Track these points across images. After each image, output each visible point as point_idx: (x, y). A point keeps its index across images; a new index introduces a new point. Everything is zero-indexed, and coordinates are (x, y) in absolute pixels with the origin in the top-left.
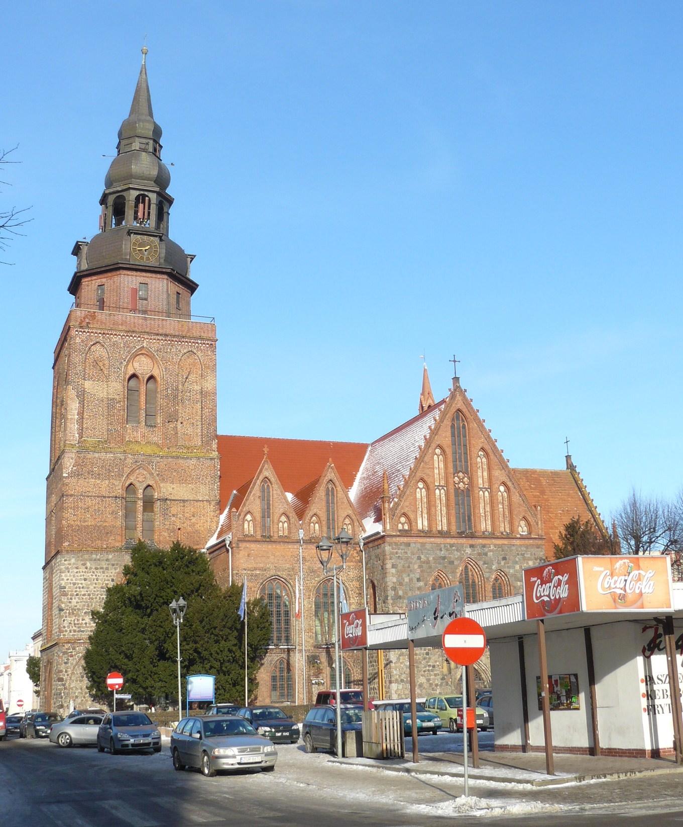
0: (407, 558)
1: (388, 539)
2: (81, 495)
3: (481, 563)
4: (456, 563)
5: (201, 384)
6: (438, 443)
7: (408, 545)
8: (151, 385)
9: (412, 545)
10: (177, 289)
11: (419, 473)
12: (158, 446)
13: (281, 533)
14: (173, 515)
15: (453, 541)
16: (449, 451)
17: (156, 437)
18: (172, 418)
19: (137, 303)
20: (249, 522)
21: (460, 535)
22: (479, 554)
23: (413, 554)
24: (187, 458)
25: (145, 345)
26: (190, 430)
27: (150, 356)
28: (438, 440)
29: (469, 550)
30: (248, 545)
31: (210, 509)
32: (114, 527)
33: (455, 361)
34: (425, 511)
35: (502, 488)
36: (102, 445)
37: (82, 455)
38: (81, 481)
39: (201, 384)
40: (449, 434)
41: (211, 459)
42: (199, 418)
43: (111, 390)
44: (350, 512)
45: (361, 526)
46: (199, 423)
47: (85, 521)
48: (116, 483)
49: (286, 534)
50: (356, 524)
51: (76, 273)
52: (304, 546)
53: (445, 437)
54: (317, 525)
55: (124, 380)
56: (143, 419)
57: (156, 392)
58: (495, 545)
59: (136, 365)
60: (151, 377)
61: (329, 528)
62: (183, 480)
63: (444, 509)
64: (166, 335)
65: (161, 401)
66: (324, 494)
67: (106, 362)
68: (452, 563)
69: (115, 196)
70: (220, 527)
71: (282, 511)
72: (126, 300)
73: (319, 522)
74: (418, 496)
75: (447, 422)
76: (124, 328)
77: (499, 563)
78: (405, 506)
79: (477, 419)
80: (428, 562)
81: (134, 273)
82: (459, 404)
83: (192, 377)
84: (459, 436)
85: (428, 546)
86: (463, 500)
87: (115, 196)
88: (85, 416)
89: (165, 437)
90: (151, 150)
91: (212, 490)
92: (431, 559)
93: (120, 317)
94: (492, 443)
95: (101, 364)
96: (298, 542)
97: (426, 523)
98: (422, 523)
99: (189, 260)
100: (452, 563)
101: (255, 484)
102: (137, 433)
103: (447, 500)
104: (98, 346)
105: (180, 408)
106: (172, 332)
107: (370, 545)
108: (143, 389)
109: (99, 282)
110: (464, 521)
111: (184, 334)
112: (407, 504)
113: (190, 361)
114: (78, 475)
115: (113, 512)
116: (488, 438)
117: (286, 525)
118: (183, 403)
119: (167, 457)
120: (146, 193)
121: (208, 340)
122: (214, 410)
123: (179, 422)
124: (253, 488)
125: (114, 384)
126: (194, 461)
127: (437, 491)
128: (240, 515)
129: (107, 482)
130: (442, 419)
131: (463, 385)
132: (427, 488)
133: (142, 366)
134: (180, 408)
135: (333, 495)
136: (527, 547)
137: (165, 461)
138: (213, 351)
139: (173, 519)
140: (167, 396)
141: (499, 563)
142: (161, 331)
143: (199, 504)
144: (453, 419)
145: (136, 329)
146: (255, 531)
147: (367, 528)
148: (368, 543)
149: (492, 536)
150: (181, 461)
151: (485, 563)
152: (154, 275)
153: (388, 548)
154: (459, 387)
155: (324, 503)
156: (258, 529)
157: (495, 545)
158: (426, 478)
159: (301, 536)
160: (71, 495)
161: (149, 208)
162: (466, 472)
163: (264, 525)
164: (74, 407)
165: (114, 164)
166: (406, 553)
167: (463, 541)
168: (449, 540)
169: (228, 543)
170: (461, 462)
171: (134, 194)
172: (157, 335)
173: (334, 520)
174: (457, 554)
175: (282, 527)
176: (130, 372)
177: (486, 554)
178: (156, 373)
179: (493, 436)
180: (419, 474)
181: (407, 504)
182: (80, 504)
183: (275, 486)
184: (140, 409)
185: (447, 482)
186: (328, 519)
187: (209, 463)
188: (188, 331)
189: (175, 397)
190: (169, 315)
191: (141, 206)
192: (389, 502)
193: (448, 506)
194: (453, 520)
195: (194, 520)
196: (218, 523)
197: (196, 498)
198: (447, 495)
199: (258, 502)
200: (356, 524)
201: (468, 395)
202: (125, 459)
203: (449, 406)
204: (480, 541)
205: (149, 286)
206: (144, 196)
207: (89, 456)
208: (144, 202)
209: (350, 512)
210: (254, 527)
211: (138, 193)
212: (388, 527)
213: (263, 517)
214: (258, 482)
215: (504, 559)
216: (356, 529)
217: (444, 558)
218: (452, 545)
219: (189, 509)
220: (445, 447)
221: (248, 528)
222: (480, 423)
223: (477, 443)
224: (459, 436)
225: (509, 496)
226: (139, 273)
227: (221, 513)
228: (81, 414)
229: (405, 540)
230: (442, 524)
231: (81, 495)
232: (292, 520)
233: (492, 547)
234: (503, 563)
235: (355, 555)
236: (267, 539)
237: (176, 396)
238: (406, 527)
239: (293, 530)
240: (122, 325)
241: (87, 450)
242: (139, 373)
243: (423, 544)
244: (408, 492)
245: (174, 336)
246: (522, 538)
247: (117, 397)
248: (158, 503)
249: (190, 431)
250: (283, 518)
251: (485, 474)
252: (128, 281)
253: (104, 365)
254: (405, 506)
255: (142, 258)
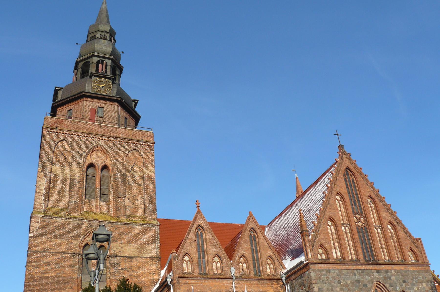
0: (330, 283)
1: (312, 266)
2: (44, 251)
3: (387, 285)
4: (369, 285)
5: (143, 172)
6: (338, 190)
7: (329, 271)
8: (105, 173)
9: (332, 271)
10: (125, 115)
11: (326, 215)
12: (110, 216)
13: (215, 272)
14: (122, 269)
15: (363, 267)
16: (347, 197)
17: (109, 209)
18: (121, 196)
19: (94, 116)
20: (187, 262)
21: (368, 263)
22: (385, 278)
23: (333, 278)
24: (133, 224)
25: (100, 143)
26: (135, 204)
27: (104, 151)
28: (337, 188)
29: (376, 275)
30: (187, 281)
31: (153, 264)
32: (71, 278)
33: (338, 135)
34: (336, 244)
35: (389, 227)
36: (63, 213)
37: (47, 220)
38: (45, 240)
39: (143, 172)
40: (344, 184)
41: (153, 225)
42: (142, 196)
43: (73, 173)
44: (271, 253)
45: (281, 264)
46: (142, 200)
47: (46, 273)
48: (74, 242)
49: (220, 272)
50: (277, 263)
51: (53, 104)
52: (237, 282)
53: (341, 187)
54: (245, 265)
55: (83, 166)
56: (98, 195)
57: (109, 177)
58: (395, 270)
59: (93, 157)
60: (105, 167)
61: (255, 267)
62: (130, 241)
63: (351, 242)
64: (116, 138)
65: (112, 183)
66: (248, 239)
67: (70, 154)
68: (365, 285)
69: (83, 62)
70: (161, 278)
71: (214, 252)
72: (87, 115)
73: (247, 262)
74: (329, 231)
75: (341, 176)
76: (84, 131)
77: (401, 286)
78: (321, 239)
79: (361, 175)
80: (347, 285)
81: (94, 100)
82: (346, 163)
83: (137, 167)
84: (351, 187)
85: (344, 272)
86: (363, 234)
87: (83, 62)
88: (51, 191)
89: (116, 208)
90: (108, 38)
91: (154, 249)
92: (349, 282)
93: (82, 124)
94: (377, 192)
95: (66, 155)
96: (231, 278)
97: (339, 254)
98: (336, 254)
99: (134, 103)
100: (365, 285)
101: (191, 230)
102: (93, 206)
103: (352, 234)
104: (64, 142)
105: (127, 188)
106: (121, 136)
107: (293, 277)
108: (98, 173)
109: (69, 108)
110: (367, 252)
111: (130, 137)
112: (322, 237)
113: (135, 156)
114: (42, 235)
115: (71, 266)
116: (372, 188)
117: (219, 265)
118: (129, 185)
119: (117, 223)
120: (104, 59)
121: (147, 142)
122: (153, 190)
123: (126, 198)
124: (189, 233)
125: (76, 169)
126: (139, 227)
127: (343, 228)
128: (179, 255)
129: (67, 241)
130: (337, 174)
131: (347, 149)
132: (335, 225)
133: (98, 159)
134: (127, 188)
135: (255, 240)
136: (418, 271)
137: (115, 226)
138: (152, 150)
139: (122, 271)
140: (117, 179)
141: (401, 286)
142: (112, 135)
143: (143, 259)
144: (344, 175)
145: (94, 132)
146: (193, 269)
147: (286, 266)
148: (290, 276)
149: (391, 263)
150: (128, 226)
151: (391, 286)
152: (108, 102)
153: (312, 274)
154: (345, 151)
155: (249, 246)
156: (195, 267)
157: (395, 270)
158: (333, 217)
159: (233, 272)
160: (35, 251)
161: (106, 68)
162: (361, 214)
163: (200, 265)
164: (42, 184)
165: (82, 47)
166: (328, 278)
167: (370, 267)
168: (360, 267)
169: (169, 280)
170: (355, 204)
171: (95, 59)
172: (110, 137)
173: (258, 260)
174: (368, 278)
175: (216, 266)
176: (89, 161)
177: (390, 278)
178: (109, 163)
179: (376, 187)
180: (327, 214)
181: (322, 237)
182: (42, 259)
183: (207, 232)
184: (96, 188)
185: (349, 220)
186: (254, 260)
187: (150, 228)
188: (133, 135)
189: (123, 180)
190: (119, 124)
191: (100, 65)
192: (308, 235)
193: (353, 239)
194: (360, 251)
195: (139, 272)
196: (159, 275)
197: (141, 255)
198: (351, 229)
199: (194, 245)
200: (277, 263)
201: (353, 157)
202: (82, 224)
203: (340, 165)
204: (384, 267)
205: (105, 109)
206: (102, 62)
207: (52, 221)
208: (102, 63)
209: (271, 253)
210: (192, 266)
211: (98, 59)
212: (310, 256)
213: (199, 258)
214: (193, 229)
215: (404, 281)
216: (277, 266)
217: (359, 282)
218: (363, 271)
219: (136, 264)
220: (343, 193)
221: (187, 267)
222: (365, 177)
223: (366, 192)
224: (351, 187)
225: (396, 233)
226: (97, 101)
227: (162, 268)
228: (48, 189)
229: (326, 266)
230: (351, 255)
231: (44, 251)
232: (224, 260)
233: (393, 272)
234: (404, 285)
235: (279, 288)
236: (204, 276)
237: (124, 180)
238: (324, 257)
239: (226, 268)
240: (83, 129)
241: (51, 216)
242: (95, 163)
243: (340, 270)
244: (321, 228)
245: (123, 138)
246: (413, 264)
247: (78, 178)
248: (110, 259)
249: (135, 205)
250: (216, 259)
251: (375, 215)
252: (89, 105)
253: (68, 155)
254: (321, 239)
255: (100, 91)
